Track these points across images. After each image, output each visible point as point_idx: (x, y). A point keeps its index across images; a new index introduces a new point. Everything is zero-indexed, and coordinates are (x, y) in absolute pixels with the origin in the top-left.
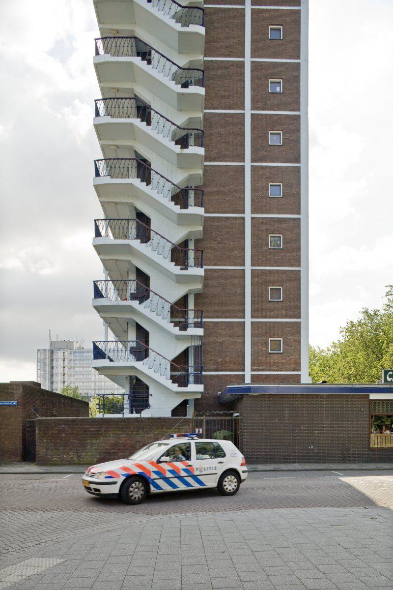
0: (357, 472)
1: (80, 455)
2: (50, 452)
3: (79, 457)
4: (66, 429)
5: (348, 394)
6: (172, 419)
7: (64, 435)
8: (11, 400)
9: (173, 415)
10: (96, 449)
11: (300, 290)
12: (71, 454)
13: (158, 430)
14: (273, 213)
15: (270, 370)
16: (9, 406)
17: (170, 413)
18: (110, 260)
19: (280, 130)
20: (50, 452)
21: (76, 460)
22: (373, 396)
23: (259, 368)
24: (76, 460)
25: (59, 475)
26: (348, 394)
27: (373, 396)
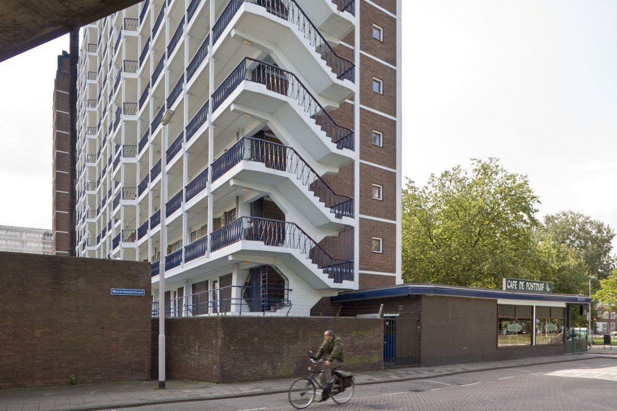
0: (554, 364)
1: (276, 367)
2: (239, 364)
3: (274, 368)
4: (259, 331)
5: (484, 298)
6: (310, 318)
7: (256, 339)
8: (134, 288)
9: (311, 314)
10: (293, 358)
11: (395, 192)
12: (265, 366)
13: (354, 332)
14: (376, 109)
15: (373, 270)
16: (132, 297)
17: (309, 312)
18: (247, 114)
19: (381, 27)
20: (239, 364)
21: (270, 372)
22: (500, 301)
23: (365, 267)
24: (270, 372)
25: (192, 397)
26: (484, 298)
27: (500, 301)
